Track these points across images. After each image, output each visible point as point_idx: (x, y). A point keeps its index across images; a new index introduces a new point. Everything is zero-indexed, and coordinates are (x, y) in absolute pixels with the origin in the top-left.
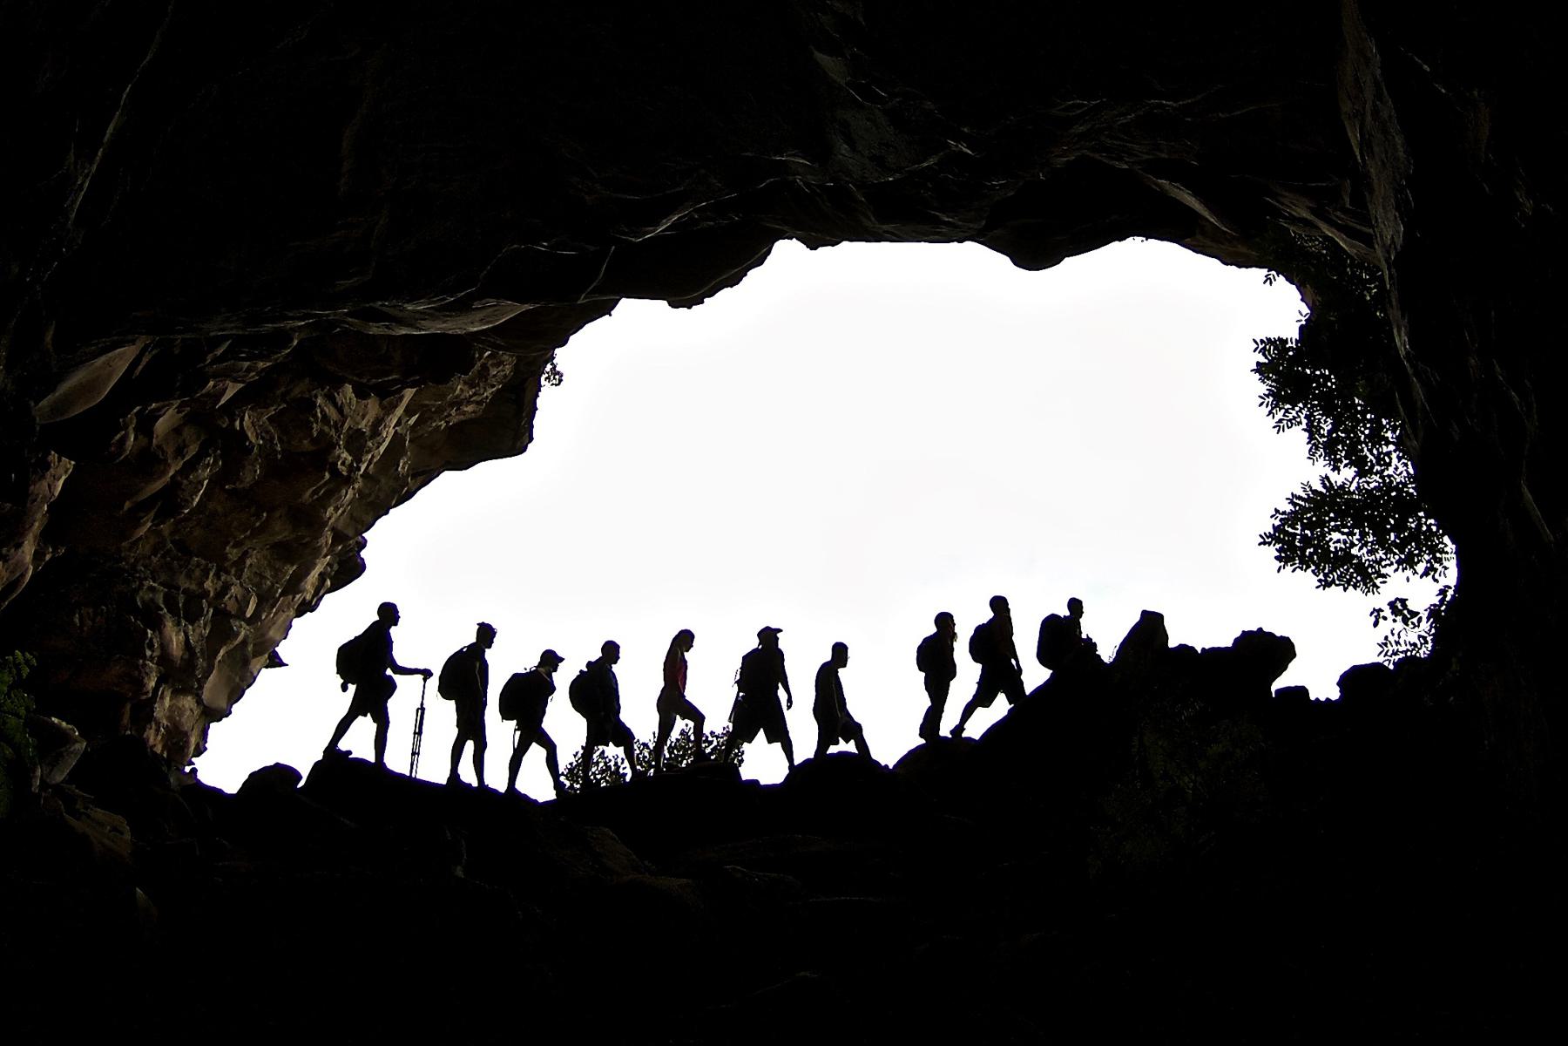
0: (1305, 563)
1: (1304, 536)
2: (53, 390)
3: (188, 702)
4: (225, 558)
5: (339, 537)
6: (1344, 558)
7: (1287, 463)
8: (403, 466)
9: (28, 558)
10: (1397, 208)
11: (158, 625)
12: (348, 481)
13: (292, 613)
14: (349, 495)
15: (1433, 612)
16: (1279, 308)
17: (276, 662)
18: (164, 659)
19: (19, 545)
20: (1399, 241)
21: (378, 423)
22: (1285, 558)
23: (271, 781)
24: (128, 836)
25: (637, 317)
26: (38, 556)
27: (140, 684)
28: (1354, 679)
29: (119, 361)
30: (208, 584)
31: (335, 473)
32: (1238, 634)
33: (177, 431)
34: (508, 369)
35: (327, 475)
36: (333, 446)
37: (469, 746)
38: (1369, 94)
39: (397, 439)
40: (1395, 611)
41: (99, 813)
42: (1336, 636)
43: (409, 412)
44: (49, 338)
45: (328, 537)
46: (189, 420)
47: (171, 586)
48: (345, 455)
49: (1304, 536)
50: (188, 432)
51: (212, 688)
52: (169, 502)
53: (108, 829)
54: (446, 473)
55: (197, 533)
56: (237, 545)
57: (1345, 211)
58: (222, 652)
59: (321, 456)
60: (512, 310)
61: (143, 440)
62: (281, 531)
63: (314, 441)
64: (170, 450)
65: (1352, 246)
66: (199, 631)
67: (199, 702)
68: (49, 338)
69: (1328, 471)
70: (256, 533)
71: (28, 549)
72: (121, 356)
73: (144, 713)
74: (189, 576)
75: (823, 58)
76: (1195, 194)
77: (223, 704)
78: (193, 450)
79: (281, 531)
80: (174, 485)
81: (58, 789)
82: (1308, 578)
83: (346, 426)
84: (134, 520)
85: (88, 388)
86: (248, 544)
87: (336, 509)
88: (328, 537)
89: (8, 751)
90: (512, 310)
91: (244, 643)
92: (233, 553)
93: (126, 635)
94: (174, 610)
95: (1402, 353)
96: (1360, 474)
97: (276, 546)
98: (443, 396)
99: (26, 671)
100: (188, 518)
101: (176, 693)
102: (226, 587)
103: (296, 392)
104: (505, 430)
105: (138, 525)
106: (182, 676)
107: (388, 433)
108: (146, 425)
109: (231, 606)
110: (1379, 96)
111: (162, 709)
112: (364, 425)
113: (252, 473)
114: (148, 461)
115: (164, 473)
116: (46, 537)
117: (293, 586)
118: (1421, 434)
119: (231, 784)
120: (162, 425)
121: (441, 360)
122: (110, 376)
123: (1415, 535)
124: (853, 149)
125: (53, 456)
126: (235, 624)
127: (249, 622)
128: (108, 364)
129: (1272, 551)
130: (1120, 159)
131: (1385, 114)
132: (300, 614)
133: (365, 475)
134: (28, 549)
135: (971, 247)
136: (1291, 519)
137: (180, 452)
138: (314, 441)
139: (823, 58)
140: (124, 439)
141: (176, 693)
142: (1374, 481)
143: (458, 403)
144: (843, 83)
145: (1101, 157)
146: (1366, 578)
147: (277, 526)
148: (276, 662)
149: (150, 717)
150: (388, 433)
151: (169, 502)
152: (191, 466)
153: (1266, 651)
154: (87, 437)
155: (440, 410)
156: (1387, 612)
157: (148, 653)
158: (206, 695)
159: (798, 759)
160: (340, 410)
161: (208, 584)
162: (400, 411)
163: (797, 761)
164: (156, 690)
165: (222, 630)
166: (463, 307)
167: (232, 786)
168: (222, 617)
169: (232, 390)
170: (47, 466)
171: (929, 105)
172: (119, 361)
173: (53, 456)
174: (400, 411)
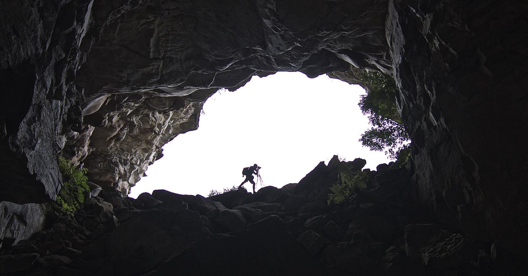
0: (368, 145)
1: (368, 140)
2: (86, 107)
3: (126, 183)
4: (132, 152)
5: (157, 147)
6: (376, 144)
7: (364, 123)
9: (86, 150)
10: (400, 53)
11: (118, 166)
12: (158, 134)
14: (159, 138)
15: (397, 153)
16: (327, 164)
18: (120, 173)
19: (83, 147)
20: (400, 62)
21: (164, 122)
22: (364, 144)
23: (144, 196)
24: (112, 207)
25: (223, 94)
26: (88, 150)
27: (115, 179)
28: (380, 167)
29: (102, 100)
30: (128, 157)
31: (155, 133)
33: (118, 121)
34: (193, 111)
36: (154, 127)
38: (395, 26)
39: (169, 126)
40: (390, 152)
41: (105, 202)
42: (375, 159)
43: (171, 120)
44: (83, 92)
45: (154, 147)
46: (121, 119)
47: (120, 158)
49: (368, 140)
50: (120, 122)
51: (131, 180)
52: (117, 138)
53: (107, 206)
55: (125, 146)
56: (134, 149)
57: (384, 60)
59: (152, 129)
60: (194, 90)
61: (110, 123)
62: (144, 146)
63: (150, 126)
64: (117, 126)
65: (384, 70)
66: (127, 167)
67: (128, 183)
68: (83, 92)
69: (372, 126)
70: (138, 146)
71: (86, 148)
72: (102, 99)
73: (116, 185)
74: (124, 156)
75: (265, 21)
76: (350, 58)
78: (122, 126)
79: (144, 146)
80: (118, 134)
81: (95, 198)
82: (369, 148)
84: (110, 141)
85: (94, 107)
86: (137, 149)
88: (154, 147)
89: (83, 190)
90: (194, 90)
91: (137, 170)
92: (133, 151)
93: (111, 168)
94: (121, 163)
95: (400, 88)
96: (379, 127)
97: (143, 149)
98: (178, 116)
99: (86, 172)
100: (122, 141)
101: (123, 181)
102: (132, 158)
103: (145, 112)
104: (192, 124)
105: (111, 143)
106: (124, 177)
107: (167, 124)
108: (111, 119)
109: (134, 162)
110: (397, 26)
111: (120, 184)
112: (161, 122)
113: (136, 131)
114: (112, 128)
115: (116, 131)
116: (90, 145)
117: (147, 158)
118: (402, 108)
119: (135, 197)
120: (115, 120)
121: (177, 104)
122: (100, 104)
123: (390, 140)
124: (272, 46)
125: (89, 126)
126: (135, 166)
127: (138, 166)
128: (99, 101)
129: (362, 142)
130: (333, 49)
131: (399, 31)
133: (162, 134)
134: (86, 148)
135: (298, 73)
136: (366, 136)
137: (119, 126)
138: (150, 126)
139: (265, 21)
140: (105, 121)
141: (123, 181)
142: (382, 128)
143: (182, 118)
144: (270, 27)
145: (328, 49)
146: (380, 148)
147: (143, 145)
149: (117, 186)
150: (167, 124)
151: (117, 138)
152: (122, 129)
153: (361, 162)
154: (96, 119)
155: (178, 120)
156: (388, 152)
158: (130, 181)
160: (156, 119)
161: (128, 157)
162: (169, 119)
164: (118, 180)
165: (132, 167)
166: (180, 88)
167: (135, 197)
168: (132, 164)
169: (130, 111)
170: (88, 128)
171: (290, 33)
172: (102, 100)
173: (89, 126)
174: (169, 119)
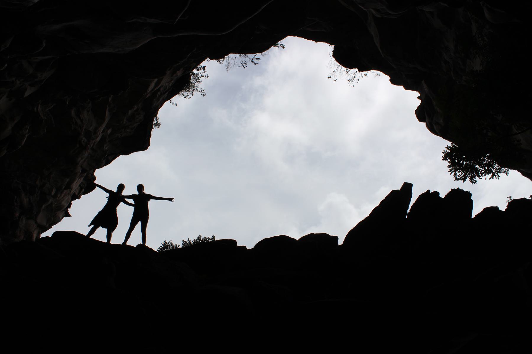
5: (84, 171)
8: (106, 147)
13: (70, 197)
17: (68, 215)
32: (193, 238)
35: (78, 146)
37: (139, 225)
39: (103, 140)
43: (107, 127)
45: (79, 170)
48: (84, 138)
54: (121, 156)
58: (43, 206)
67: (36, 222)
77: (44, 223)
83: (84, 127)
87: (82, 159)
91: (52, 204)
117: (69, 186)
132: (74, 199)
148: (68, 215)
157: (15, 204)
159: (128, 243)
162: (104, 125)
163: (92, 237)
174: (104, 125)
